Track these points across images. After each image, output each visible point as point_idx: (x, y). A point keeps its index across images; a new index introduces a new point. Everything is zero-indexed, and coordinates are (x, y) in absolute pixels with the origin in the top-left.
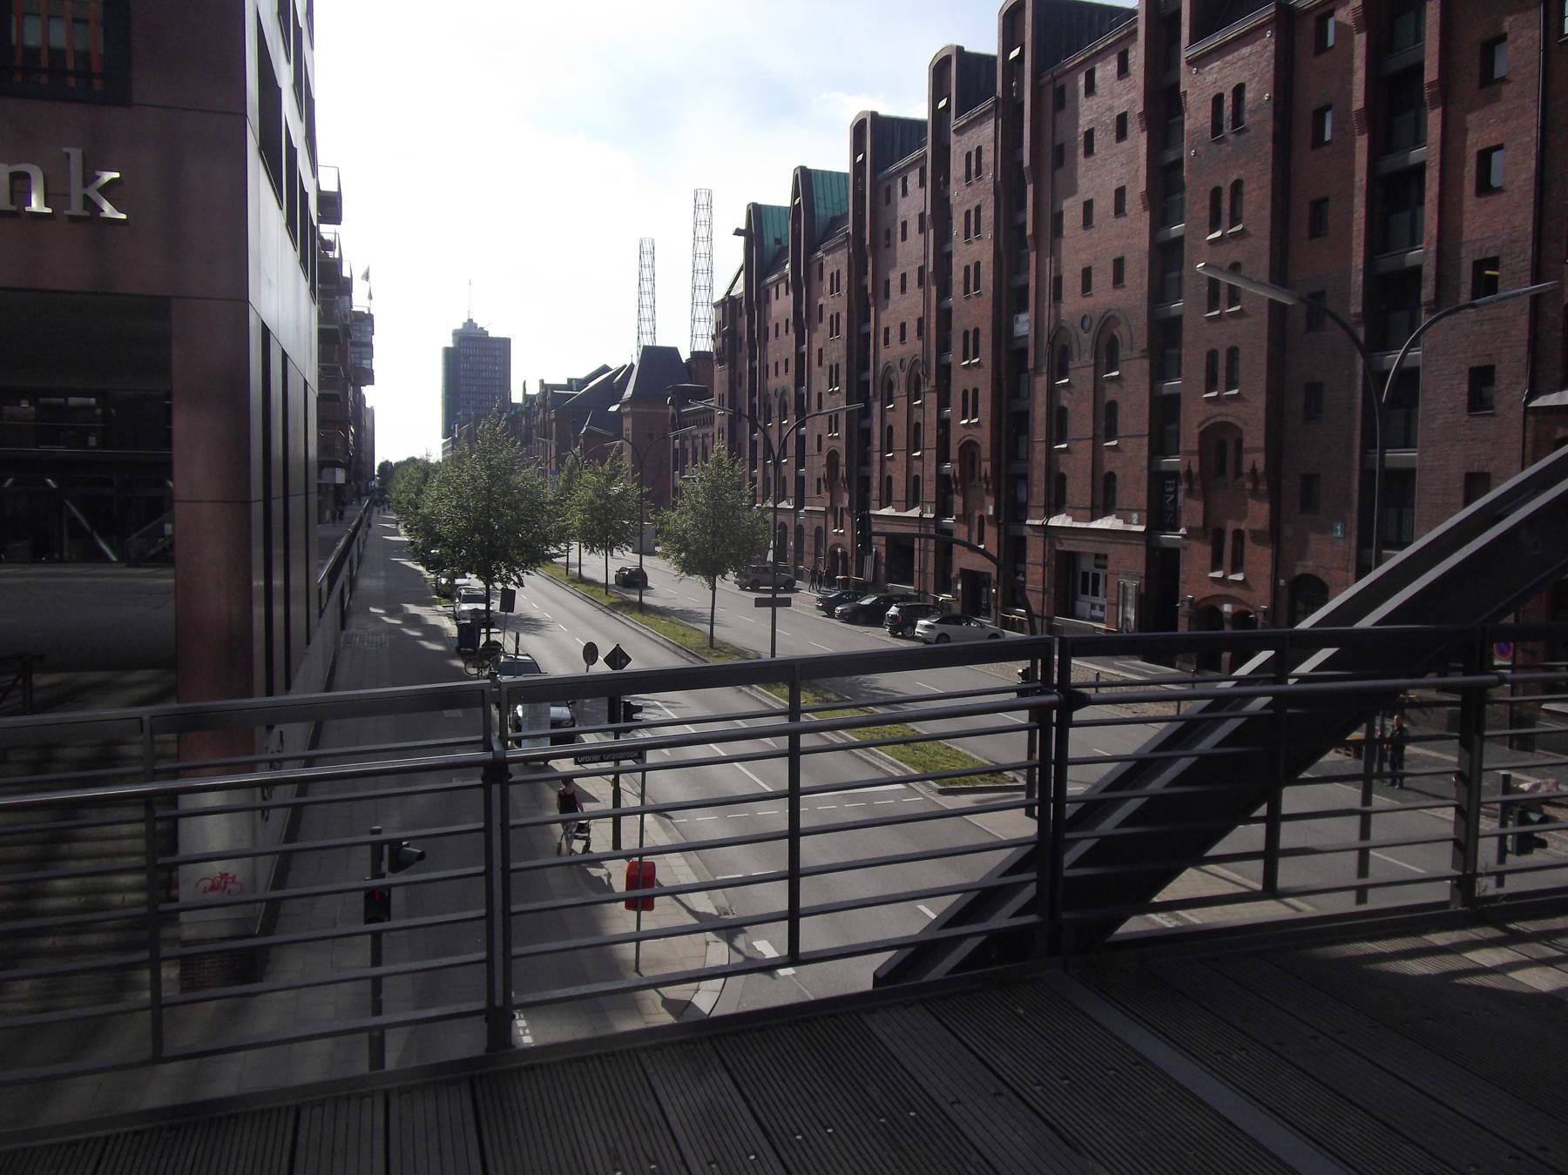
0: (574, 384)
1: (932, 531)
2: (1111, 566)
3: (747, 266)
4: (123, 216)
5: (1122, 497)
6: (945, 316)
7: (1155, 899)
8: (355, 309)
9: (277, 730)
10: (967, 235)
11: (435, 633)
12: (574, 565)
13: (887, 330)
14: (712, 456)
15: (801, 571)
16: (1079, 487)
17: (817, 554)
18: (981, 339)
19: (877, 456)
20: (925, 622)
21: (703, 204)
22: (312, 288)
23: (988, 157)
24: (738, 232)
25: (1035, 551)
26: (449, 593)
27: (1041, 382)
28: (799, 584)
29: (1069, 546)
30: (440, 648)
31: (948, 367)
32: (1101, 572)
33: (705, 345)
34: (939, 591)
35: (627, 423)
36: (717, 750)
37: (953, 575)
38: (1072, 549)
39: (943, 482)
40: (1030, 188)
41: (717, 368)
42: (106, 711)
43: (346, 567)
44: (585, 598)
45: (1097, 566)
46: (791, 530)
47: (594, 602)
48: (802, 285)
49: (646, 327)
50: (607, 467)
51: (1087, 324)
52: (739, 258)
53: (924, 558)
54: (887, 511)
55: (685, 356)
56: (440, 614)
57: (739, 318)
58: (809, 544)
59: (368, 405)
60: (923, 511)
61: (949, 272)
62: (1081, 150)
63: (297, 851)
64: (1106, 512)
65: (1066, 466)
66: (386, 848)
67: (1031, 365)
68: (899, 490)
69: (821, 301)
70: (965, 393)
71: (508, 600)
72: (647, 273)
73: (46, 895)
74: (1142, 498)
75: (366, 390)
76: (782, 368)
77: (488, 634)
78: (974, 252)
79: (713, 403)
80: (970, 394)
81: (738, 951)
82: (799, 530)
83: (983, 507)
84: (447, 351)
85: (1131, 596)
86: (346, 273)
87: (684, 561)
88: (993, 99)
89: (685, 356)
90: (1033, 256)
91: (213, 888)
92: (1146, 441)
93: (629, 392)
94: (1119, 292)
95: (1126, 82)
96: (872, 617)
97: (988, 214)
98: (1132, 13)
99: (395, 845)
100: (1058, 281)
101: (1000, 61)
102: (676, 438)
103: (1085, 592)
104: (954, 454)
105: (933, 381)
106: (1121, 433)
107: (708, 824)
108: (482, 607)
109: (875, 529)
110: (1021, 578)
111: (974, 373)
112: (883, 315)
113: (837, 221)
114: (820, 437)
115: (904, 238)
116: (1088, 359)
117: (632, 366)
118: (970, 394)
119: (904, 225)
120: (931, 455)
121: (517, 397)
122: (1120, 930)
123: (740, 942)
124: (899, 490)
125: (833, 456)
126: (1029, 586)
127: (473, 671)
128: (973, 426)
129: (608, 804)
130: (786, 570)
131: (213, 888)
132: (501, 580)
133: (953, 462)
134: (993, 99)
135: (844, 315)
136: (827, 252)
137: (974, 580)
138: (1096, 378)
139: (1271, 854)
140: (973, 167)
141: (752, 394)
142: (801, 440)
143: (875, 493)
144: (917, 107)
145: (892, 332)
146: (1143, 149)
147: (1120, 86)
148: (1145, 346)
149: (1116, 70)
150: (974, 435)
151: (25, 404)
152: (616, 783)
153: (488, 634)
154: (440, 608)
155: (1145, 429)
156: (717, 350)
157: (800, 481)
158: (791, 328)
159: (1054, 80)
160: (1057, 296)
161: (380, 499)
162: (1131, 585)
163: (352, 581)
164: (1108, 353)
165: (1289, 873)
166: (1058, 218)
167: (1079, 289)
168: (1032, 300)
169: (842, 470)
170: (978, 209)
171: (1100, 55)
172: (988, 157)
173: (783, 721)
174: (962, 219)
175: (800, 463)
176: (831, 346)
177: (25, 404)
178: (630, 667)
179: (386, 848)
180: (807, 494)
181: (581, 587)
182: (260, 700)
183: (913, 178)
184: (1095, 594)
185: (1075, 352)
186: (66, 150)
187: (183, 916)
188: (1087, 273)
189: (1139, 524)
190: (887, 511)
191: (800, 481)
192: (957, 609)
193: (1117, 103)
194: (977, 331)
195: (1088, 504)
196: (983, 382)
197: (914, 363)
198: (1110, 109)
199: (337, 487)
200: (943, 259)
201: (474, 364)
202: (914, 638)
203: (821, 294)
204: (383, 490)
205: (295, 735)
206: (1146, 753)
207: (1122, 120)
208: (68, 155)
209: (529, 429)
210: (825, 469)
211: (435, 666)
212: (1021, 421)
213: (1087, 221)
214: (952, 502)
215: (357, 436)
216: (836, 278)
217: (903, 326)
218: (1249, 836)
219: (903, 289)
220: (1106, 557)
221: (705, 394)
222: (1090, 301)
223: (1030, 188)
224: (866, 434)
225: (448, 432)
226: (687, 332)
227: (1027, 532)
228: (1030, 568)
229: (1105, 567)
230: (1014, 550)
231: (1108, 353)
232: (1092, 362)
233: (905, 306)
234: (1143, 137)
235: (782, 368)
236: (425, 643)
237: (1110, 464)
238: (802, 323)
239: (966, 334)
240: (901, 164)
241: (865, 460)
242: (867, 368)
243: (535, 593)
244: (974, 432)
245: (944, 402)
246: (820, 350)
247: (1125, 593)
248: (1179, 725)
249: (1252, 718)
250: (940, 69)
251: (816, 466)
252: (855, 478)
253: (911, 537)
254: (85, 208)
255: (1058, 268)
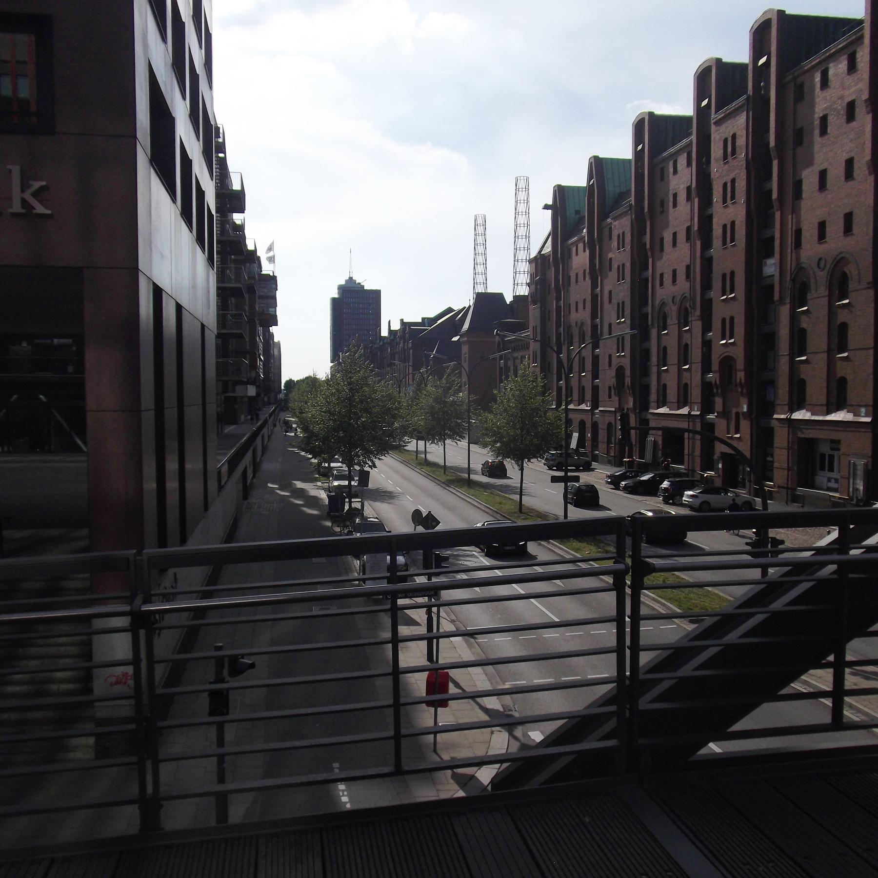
0: (426, 321)
1: (698, 428)
2: (843, 449)
3: (554, 233)
4: (49, 212)
5: (852, 395)
6: (707, 263)
7: (730, 730)
8: (263, 272)
9: (171, 572)
10: (725, 201)
11: (314, 502)
12: (421, 452)
13: (662, 275)
14: (520, 372)
15: (597, 455)
16: (816, 388)
17: (609, 442)
18: (736, 279)
19: (654, 370)
20: (691, 493)
21: (522, 187)
22: (210, 259)
23: (741, 142)
24: (546, 207)
25: (781, 438)
26: (327, 474)
27: (785, 311)
28: (594, 464)
29: (809, 434)
30: (315, 512)
31: (710, 301)
32: (835, 453)
33: (524, 291)
34: (704, 469)
35: (465, 349)
36: (519, 589)
37: (716, 457)
38: (811, 436)
39: (707, 387)
40: (775, 163)
41: (532, 307)
42: (56, 557)
43: (249, 456)
44: (428, 476)
45: (832, 449)
46: (589, 425)
47: (434, 479)
48: (596, 245)
49: (480, 279)
50: (444, 381)
51: (822, 265)
52: (548, 227)
53: (693, 446)
54: (663, 410)
55: (509, 299)
56: (319, 488)
57: (547, 270)
58: (602, 436)
59: (276, 340)
60: (691, 409)
61: (710, 229)
62: (817, 132)
63: (191, 659)
64: (838, 409)
65: (805, 373)
66: (226, 661)
67: (776, 297)
68: (672, 394)
69: (610, 255)
70: (724, 320)
71: (364, 477)
72: (480, 240)
73: (51, 681)
74: (868, 396)
75: (273, 329)
76: (581, 306)
77: (350, 502)
78: (731, 213)
79: (527, 333)
80: (728, 322)
81: (516, 738)
82: (595, 425)
83: (738, 405)
84: (334, 300)
85: (860, 472)
86: (250, 247)
87: (499, 449)
88: (745, 97)
89: (509, 299)
90: (778, 215)
91: (117, 683)
92: (871, 352)
93: (466, 326)
94: (848, 239)
95: (855, 76)
96: (649, 489)
97: (741, 185)
98: (860, 22)
99: (234, 659)
100: (798, 233)
101: (750, 67)
102: (501, 358)
103: (822, 468)
104: (715, 366)
105: (698, 312)
106: (851, 347)
107: (504, 645)
108: (346, 483)
109: (652, 424)
110: (770, 459)
111: (730, 305)
112: (659, 264)
113: (622, 196)
114: (610, 356)
115: (675, 205)
116: (823, 291)
117: (470, 306)
118: (728, 322)
119: (675, 196)
120: (697, 368)
121: (384, 333)
122: (699, 753)
123: (519, 732)
124: (672, 394)
125: (620, 371)
126: (776, 465)
127: (338, 529)
128: (730, 345)
129: (422, 630)
130: (584, 455)
131: (117, 683)
132: (359, 464)
133: (714, 372)
134: (745, 97)
135: (628, 265)
136: (615, 219)
137: (733, 461)
138: (830, 305)
139: (838, 693)
140: (729, 149)
141: (558, 325)
142: (596, 359)
143: (653, 397)
144: (682, 104)
145: (666, 277)
146: (868, 128)
147: (849, 80)
148: (870, 279)
149: (846, 68)
150: (731, 352)
151: (24, 344)
152: (429, 613)
153: (350, 502)
154: (319, 484)
155: (871, 342)
156: (530, 293)
157: (595, 389)
158: (587, 276)
159: (795, 78)
160: (798, 244)
161: (283, 406)
162: (861, 463)
163: (256, 466)
164: (839, 285)
165: (855, 709)
166: (798, 184)
167: (816, 238)
168: (777, 249)
169: (628, 380)
170: (733, 181)
171: (832, 57)
172: (741, 142)
173: (609, 564)
174: (721, 189)
175: (595, 376)
176: (617, 288)
177: (24, 344)
178: (439, 528)
179: (226, 661)
180: (601, 399)
181: (426, 469)
182: (151, 551)
183: (682, 160)
184: (831, 469)
185: (813, 286)
186: (10, 167)
187: (97, 704)
188: (822, 226)
189: (866, 416)
190: (663, 410)
191: (595, 389)
192: (718, 483)
193: (846, 93)
194: (733, 274)
195: (824, 402)
196: (738, 311)
197: (684, 299)
198: (842, 98)
199: (251, 398)
200: (706, 221)
201: (354, 308)
202: (682, 505)
203: (610, 250)
204: (286, 400)
205: (192, 577)
206: (730, 610)
207: (851, 107)
208: (10, 171)
209: (393, 355)
210: (614, 380)
211: (311, 525)
212: (770, 340)
213: (822, 185)
214: (714, 402)
215: (266, 363)
216: (621, 238)
217: (674, 271)
218: (820, 679)
219: (674, 244)
220: (839, 442)
221: (523, 327)
222: (824, 246)
223: (775, 163)
224: (647, 353)
225: (335, 357)
226: (509, 281)
227: (774, 423)
228: (777, 452)
229: (839, 450)
230: (763, 438)
231: (839, 285)
232: (827, 293)
233: (676, 257)
234: (868, 119)
235: (581, 306)
236: (305, 509)
237: (842, 370)
238: (596, 273)
239: (724, 276)
240: (672, 150)
241: (646, 373)
242: (646, 304)
243: (385, 471)
244: (730, 349)
245: (707, 327)
246: (610, 292)
247: (855, 469)
248: (760, 587)
249: (822, 582)
250: (702, 77)
251: (608, 377)
252: (638, 384)
253: (683, 431)
254: (23, 208)
255: (798, 222)
